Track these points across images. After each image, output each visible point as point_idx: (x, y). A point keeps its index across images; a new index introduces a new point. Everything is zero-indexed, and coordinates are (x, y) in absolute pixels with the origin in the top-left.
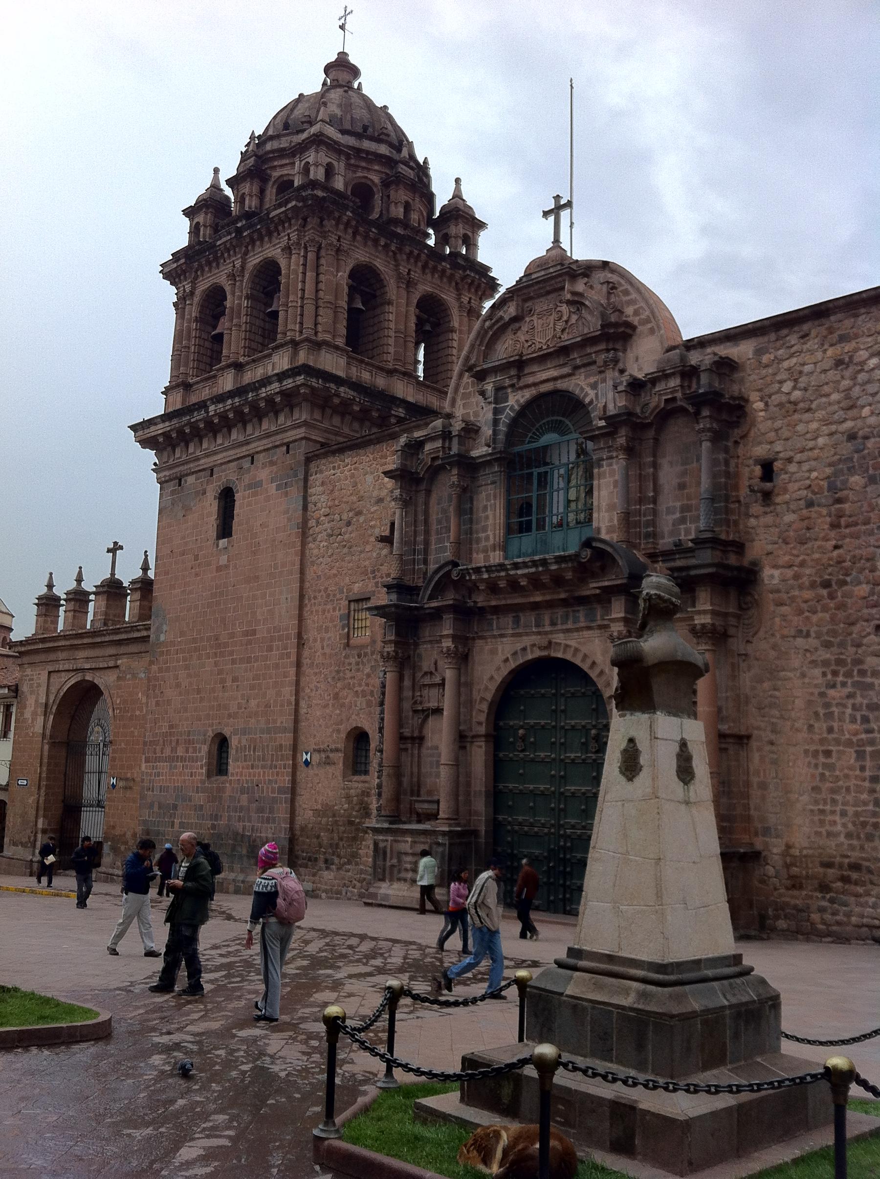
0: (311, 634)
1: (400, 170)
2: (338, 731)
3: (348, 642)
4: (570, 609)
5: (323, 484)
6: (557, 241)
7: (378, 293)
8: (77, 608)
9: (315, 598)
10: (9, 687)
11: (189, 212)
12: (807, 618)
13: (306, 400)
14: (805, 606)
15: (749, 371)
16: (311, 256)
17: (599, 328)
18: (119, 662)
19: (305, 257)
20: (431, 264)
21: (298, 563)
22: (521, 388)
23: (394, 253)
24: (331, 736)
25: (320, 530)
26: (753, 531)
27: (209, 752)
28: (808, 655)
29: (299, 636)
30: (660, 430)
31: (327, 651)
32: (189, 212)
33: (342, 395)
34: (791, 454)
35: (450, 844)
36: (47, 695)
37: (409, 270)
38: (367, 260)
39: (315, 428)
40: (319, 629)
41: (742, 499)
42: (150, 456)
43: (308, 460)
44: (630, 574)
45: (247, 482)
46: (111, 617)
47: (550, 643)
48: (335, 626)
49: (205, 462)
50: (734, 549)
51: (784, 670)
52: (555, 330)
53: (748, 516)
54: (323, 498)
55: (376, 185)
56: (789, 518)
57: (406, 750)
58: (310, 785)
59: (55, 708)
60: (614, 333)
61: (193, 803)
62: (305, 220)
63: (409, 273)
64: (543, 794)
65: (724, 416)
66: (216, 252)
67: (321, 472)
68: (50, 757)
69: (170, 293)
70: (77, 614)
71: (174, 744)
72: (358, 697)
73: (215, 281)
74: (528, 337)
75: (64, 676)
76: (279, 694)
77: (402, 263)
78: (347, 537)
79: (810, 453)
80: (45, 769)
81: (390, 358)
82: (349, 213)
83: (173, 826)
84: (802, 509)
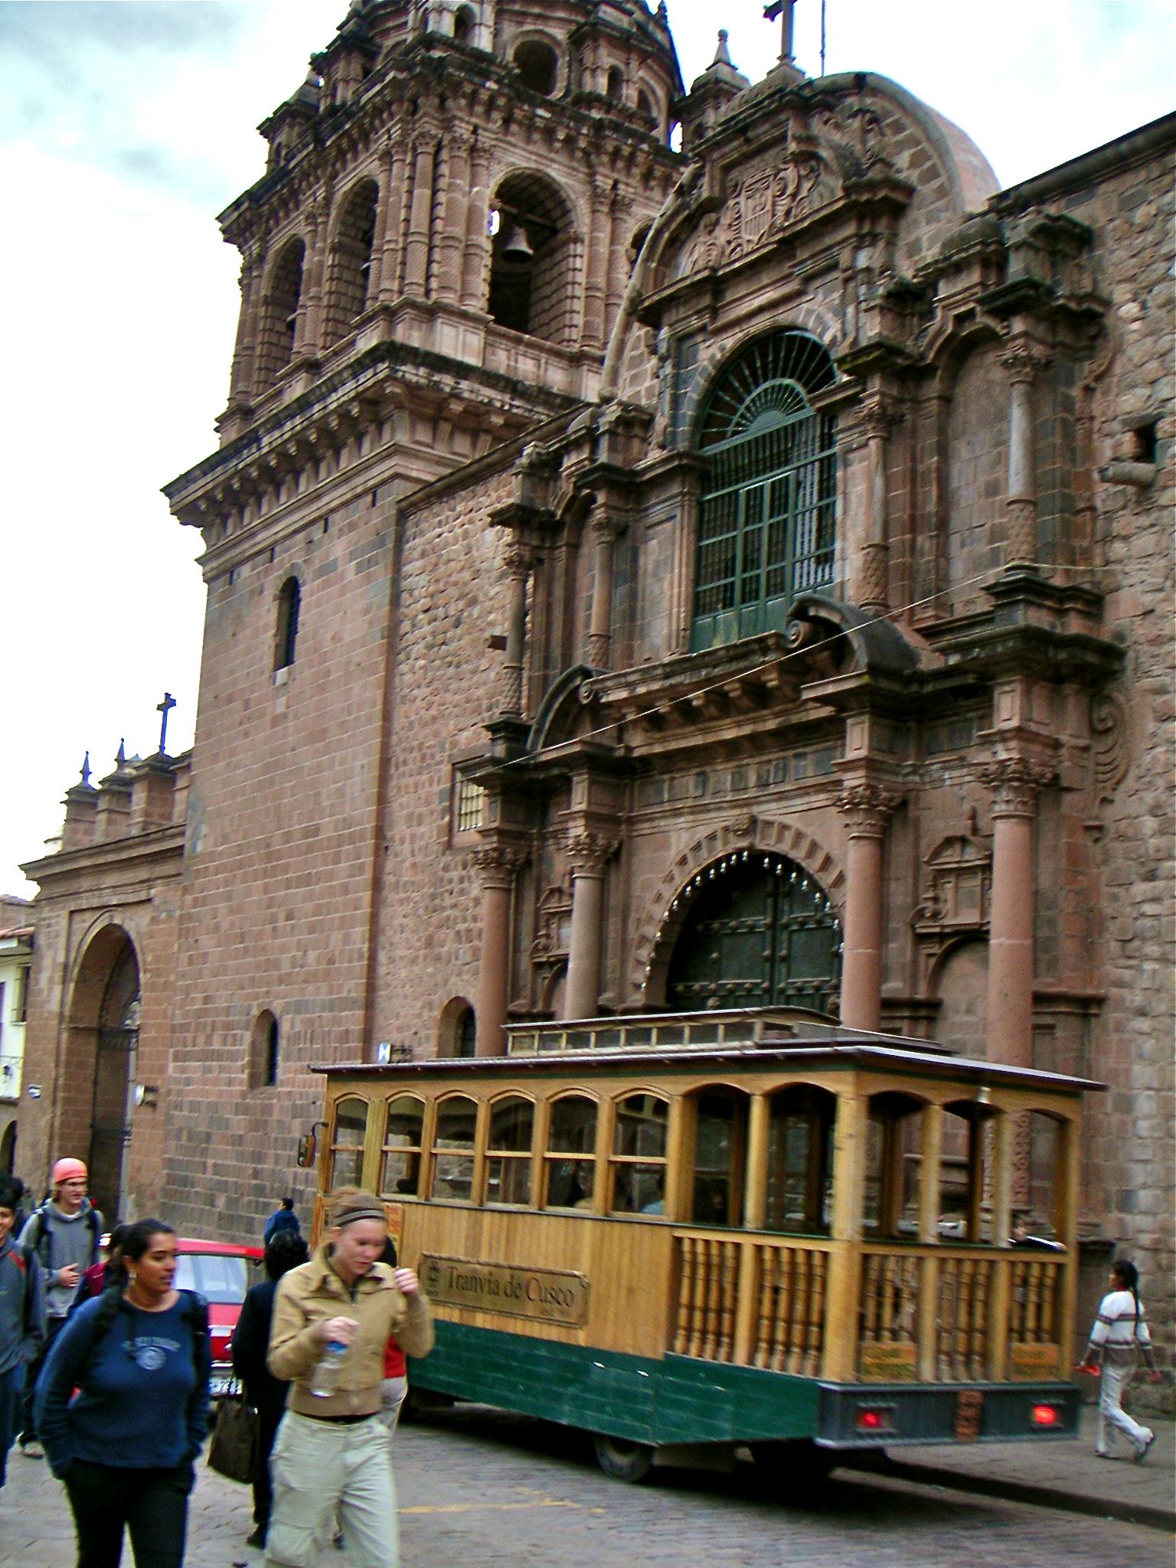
0: (399, 830)
1: (601, 14)
5: (423, 555)
6: (786, 56)
7: (560, 224)
8: (113, 807)
10: (19, 937)
13: (400, 407)
16: (424, 162)
17: (840, 194)
18: (153, 891)
19: (413, 164)
20: (659, 171)
21: (380, 701)
23: (586, 154)
24: (419, 1015)
25: (418, 635)
27: (253, 1043)
29: (380, 832)
30: (954, 377)
31: (419, 859)
32: (268, 129)
33: (466, 395)
37: (616, 183)
38: (533, 165)
42: (193, 541)
43: (405, 513)
45: (317, 564)
46: (155, 819)
47: (753, 821)
48: (432, 813)
49: (264, 538)
50: (1078, 606)
52: (774, 215)
54: (423, 580)
55: (558, 43)
59: (76, 970)
61: (231, 1133)
62: (414, 102)
63: (615, 187)
67: (422, 534)
69: (232, 258)
70: (115, 816)
74: (730, 235)
75: (89, 917)
76: (346, 940)
77: (601, 169)
78: (454, 645)
80: (62, 1071)
81: (575, 334)
82: (491, 85)
83: (277, 1156)
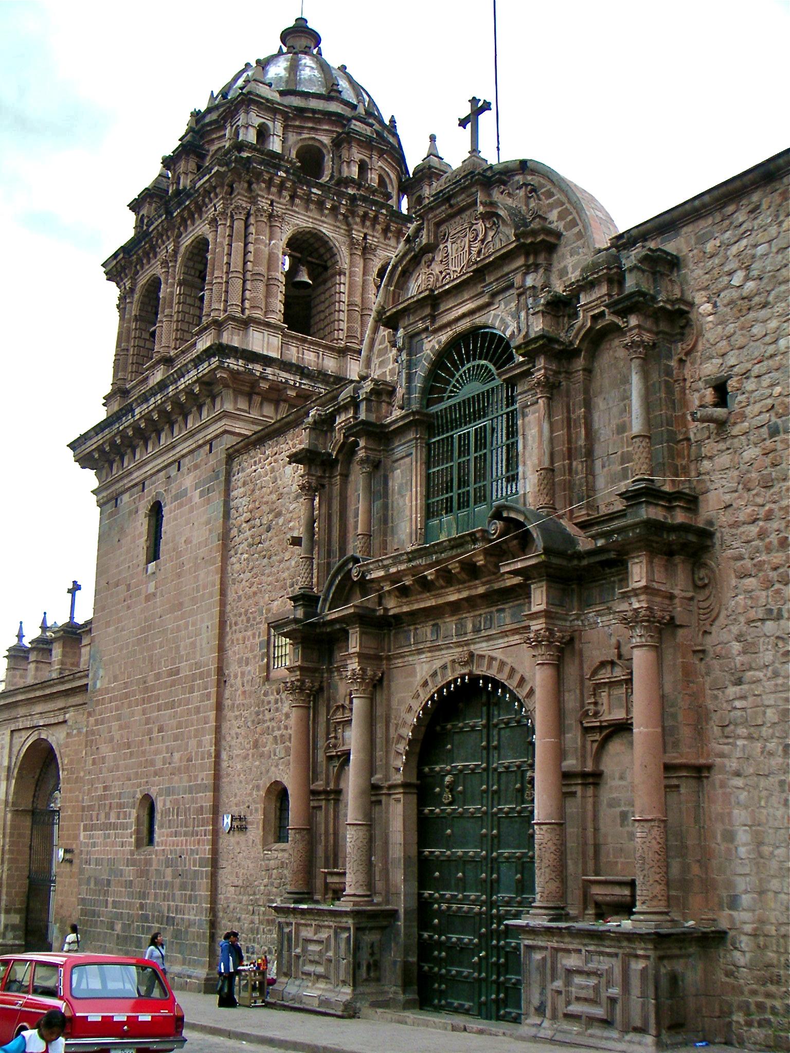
0: (233, 669)
1: (352, 126)
2: (258, 787)
3: (268, 676)
4: (494, 609)
5: (244, 484)
6: (474, 150)
7: (329, 264)
9: (236, 624)
11: (135, 206)
12: (778, 592)
13: (226, 386)
14: (773, 575)
15: (691, 266)
16: (239, 225)
19: (232, 227)
22: (436, 331)
24: (251, 794)
25: (242, 537)
26: (707, 477)
27: (138, 817)
28: (780, 644)
29: (220, 671)
32: (135, 206)
33: (270, 377)
34: (749, 366)
35: (357, 929)
36: (10, 758)
37: (366, 235)
39: (239, 419)
40: (240, 661)
41: (692, 436)
42: (90, 478)
44: (544, 549)
47: (471, 655)
49: (137, 476)
51: (751, 669)
53: (700, 458)
56: (751, 453)
57: (573, 794)
58: (231, 856)
59: (16, 771)
60: (532, 243)
61: (124, 879)
63: (365, 238)
64: (472, 860)
65: (663, 326)
66: (151, 240)
68: (13, 827)
69: (113, 291)
70: (41, 665)
71: (107, 808)
72: (276, 743)
73: (153, 273)
74: (442, 268)
75: (25, 734)
76: (200, 744)
79: (771, 362)
80: (7, 840)
84: (765, 440)
